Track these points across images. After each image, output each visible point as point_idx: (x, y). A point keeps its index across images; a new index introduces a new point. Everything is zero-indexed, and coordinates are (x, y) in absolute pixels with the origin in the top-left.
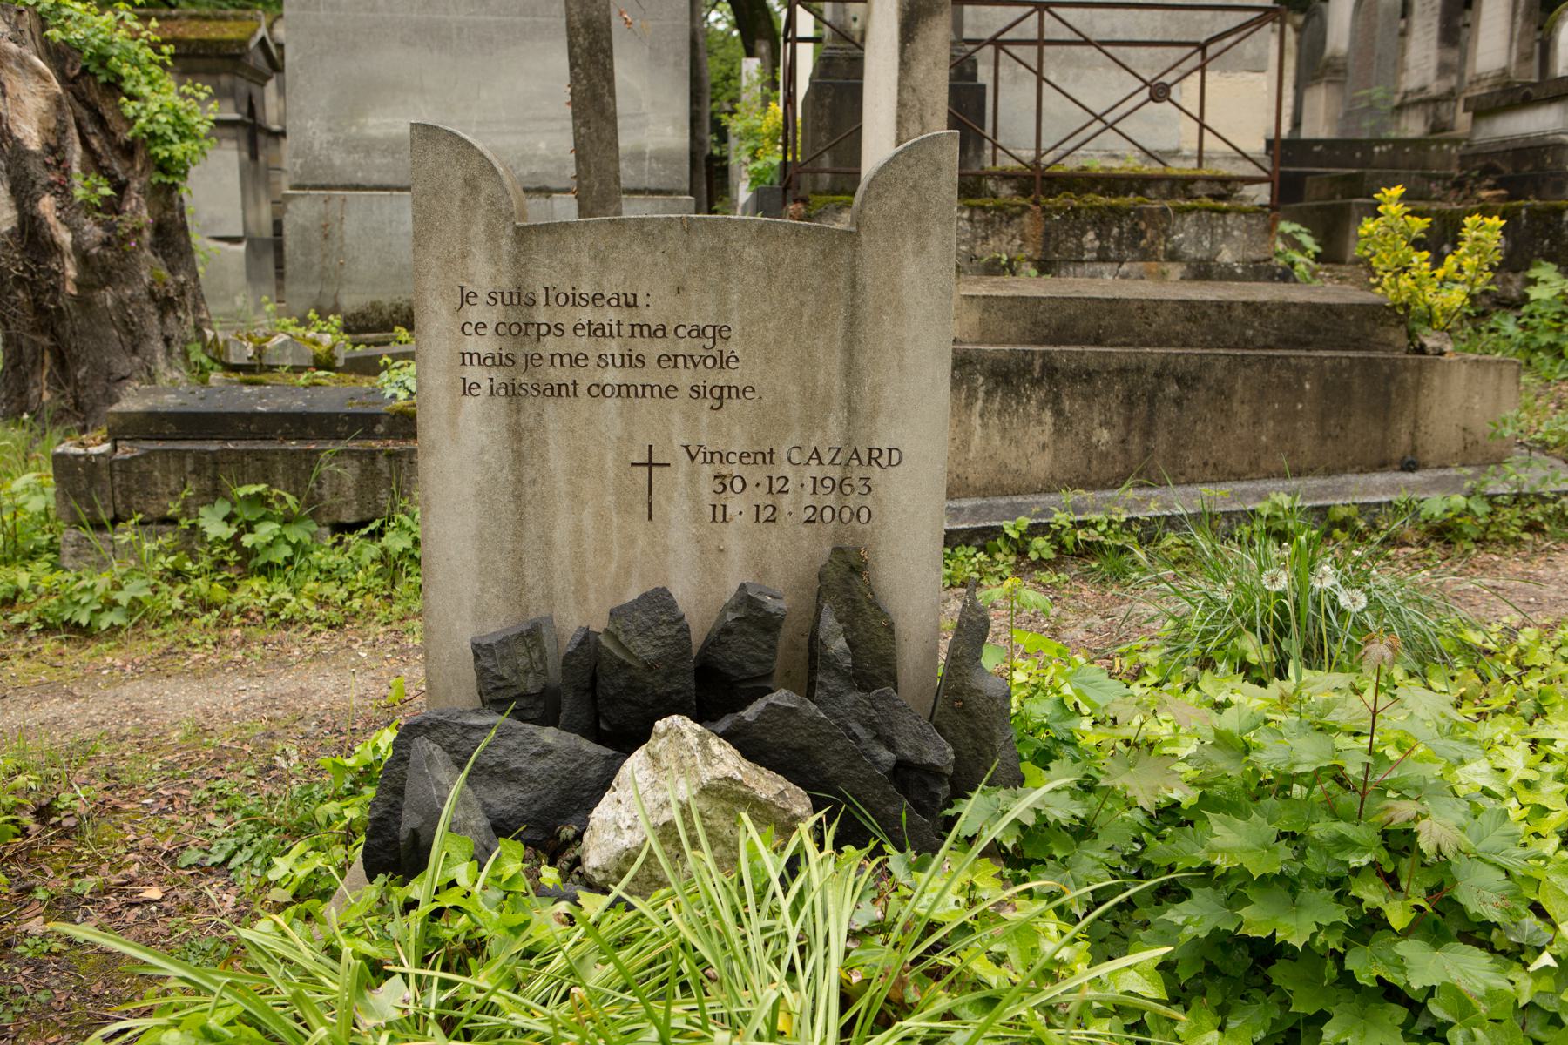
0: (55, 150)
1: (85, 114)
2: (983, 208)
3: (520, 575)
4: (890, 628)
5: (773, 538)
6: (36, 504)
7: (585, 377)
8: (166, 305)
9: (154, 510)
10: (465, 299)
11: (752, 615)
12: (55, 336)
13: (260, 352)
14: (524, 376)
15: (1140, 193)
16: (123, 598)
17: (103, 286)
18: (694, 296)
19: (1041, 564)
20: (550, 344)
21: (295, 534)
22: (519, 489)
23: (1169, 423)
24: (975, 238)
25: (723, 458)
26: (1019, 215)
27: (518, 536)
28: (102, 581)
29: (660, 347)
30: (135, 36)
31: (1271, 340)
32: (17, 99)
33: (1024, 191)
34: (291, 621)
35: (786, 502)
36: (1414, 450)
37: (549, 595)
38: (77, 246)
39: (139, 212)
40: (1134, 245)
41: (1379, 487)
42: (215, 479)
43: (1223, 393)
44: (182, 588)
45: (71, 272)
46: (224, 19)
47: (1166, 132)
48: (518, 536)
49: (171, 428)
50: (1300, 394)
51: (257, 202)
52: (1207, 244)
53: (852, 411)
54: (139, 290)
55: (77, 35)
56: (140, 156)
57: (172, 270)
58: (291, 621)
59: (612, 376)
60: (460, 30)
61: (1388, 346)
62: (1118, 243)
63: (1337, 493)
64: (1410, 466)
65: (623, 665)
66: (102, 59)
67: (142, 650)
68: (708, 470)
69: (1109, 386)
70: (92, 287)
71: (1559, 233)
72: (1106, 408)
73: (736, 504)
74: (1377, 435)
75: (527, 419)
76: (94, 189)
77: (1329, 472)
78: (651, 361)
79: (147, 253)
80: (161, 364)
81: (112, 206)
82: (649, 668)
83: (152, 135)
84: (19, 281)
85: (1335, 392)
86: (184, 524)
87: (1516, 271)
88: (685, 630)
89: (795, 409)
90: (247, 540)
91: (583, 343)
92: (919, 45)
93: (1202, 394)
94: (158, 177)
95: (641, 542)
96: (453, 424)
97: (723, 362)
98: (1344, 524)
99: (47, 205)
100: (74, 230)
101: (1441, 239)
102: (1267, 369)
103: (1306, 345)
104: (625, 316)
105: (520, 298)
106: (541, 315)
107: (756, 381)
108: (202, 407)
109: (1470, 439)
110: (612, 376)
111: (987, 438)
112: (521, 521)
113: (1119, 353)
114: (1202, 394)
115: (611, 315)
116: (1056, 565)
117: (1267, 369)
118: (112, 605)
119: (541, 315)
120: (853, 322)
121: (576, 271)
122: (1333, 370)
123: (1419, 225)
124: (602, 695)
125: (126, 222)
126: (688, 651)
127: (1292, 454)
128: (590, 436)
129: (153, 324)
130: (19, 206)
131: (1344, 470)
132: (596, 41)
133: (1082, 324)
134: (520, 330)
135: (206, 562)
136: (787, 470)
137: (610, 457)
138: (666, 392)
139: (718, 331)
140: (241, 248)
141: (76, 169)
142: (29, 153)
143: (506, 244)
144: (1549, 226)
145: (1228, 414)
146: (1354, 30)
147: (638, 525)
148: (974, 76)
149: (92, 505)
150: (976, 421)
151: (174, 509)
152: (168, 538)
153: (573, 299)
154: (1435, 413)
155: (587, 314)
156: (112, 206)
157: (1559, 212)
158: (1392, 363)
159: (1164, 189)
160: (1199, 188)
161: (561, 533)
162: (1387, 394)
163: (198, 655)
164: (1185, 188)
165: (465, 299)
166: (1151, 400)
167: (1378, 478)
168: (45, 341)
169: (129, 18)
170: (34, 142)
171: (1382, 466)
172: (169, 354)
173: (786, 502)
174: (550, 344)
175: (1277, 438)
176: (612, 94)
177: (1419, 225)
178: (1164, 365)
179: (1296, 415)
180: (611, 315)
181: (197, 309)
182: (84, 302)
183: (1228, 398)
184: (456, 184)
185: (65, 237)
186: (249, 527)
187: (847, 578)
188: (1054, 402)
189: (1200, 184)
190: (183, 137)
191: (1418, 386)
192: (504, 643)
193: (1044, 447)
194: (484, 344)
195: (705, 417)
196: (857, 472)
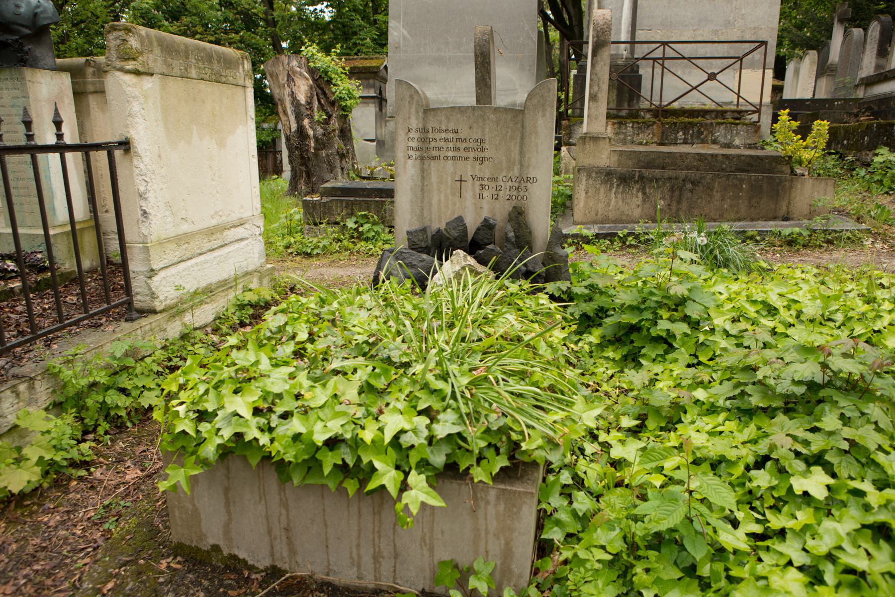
0: (309, 103)
1: (320, 91)
2: (638, 123)
3: (422, 213)
4: (530, 233)
5: (497, 205)
6: (297, 217)
7: (443, 154)
8: (342, 156)
9: (332, 219)
10: (409, 131)
11: (487, 226)
12: (307, 167)
13: (372, 172)
14: (425, 154)
15: (703, 117)
16: (321, 245)
17: (322, 149)
18: (475, 130)
19: (630, 246)
20: (433, 144)
21: (376, 228)
22: (423, 188)
23: (687, 199)
24: (634, 134)
25: (483, 179)
26: (652, 125)
27: (422, 202)
28: (315, 240)
29: (464, 145)
30: (337, 65)
31: (733, 169)
32: (299, 87)
33: (656, 116)
34: (372, 255)
35: (501, 193)
36: (788, 213)
37: (430, 220)
38: (314, 136)
39: (335, 124)
40: (698, 137)
41: (771, 226)
42: (352, 209)
43: (709, 188)
44: (339, 244)
45: (313, 145)
46: (372, 59)
47: (718, 95)
48: (422, 202)
49: (339, 193)
50: (741, 189)
51: (381, 126)
52: (729, 137)
53: (522, 165)
54: (334, 151)
55: (318, 65)
56: (337, 105)
57: (345, 145)
58: (372, 255)
59: (450, 154)
60: (450, 59)
61: (782, 172)
62: (692, 136)
63: (751, 227)
64: (786, 219)
65: (448, 239)
66: (326, 72)
67: (325, 261)
68: (478, 183)
69: (664, 184)
70: (319, 150)
71: (891, 134)
72: (663, 192)
73: (486, 194)
74: (773, 206)
75: (426, 167)
76: (321, 116)
77: (752, 220)
78: (462, 149)
79: (337, 138)
80: (340, 177)
81: (327, 122)
82: (455, 239)
83: (341, 98)
84: (297, 148)
85: (756, 190)
86: (342, 224)
87: (870, 151)
88: (466, 228)
89: (504, 164)
90: (361, 229)
91: (442, 144)
92: (599, 58)
93: (701, 188)
94: (342, 112)
95: (458, 204)
96: (405, 168)
97: (483, 150)
98: (751, 238)
99: (306, 122)
100: (314, 130)
101: (804, 131)
102: (728, 179)
103: (748, 171)
104: (454, 135)
105: (424, 130)
106: (430, 135)
107: (493, 156)
108: (349, 186)
109: (812, 209)
110: (450, 154)
111: (617, 202)
112: (423, 197)
113: (669, 173)
114: (701, 188)
115: (451, 135)
116: (636, 247)
117: (728, 179)
118: (317, 247)
119: (430, 135)
120: (522, 138)
121: (441, 122)
122: (755, 180)
123: (795, 124)
124: (440, 245)
125: (330, 128)
126: (466, 235)
127: (737, 212)
128: (444, 172)
129: (338, 163)
130: (298, 123)
131: (758, 219)
132: (484, 59)
133: (657, 161)
134: (424, 140)
135: (347, 236)
136: (502, 183)
137: (449, 178)
138: (466, 159)
139: (482, 141)
140: (375, 144)
141: (316, 110)
142: (301, 105)
143: (421, 114)
144: (887, 131)
145: (711, 196)
146: (841, 52)
147: (457, 199)
148: (638, 72)
149: (313, 217)
150: (613, 196)
151: (339, 219)
152: (337, 229)
153: (440, 131)
154: (797, 199)
155: (443, 135)
156: (327, 122)
157: (892, 125)
158: (780, 179)
159: (713, 115)
160: (728, 115)
161: (435, 201)
162: (778, 191)
163: (342, 262)
164: (722, 115)
165: (409, 131)
166: (681, 190)
167: (771, 223)
168: (304, 168)
169: (335, 58)
170: (303, 102)
171: (774, 218)
172: (343, 174)
173: (501, 193)
174: (433, 144)
175: (731, 206)
176: (490, 78)
177: (795, 124)
178: (686, 177)
179: (739, 197)
180: (451, 135)
181: (353, 159)
182: (316, 155)
183: (712, 190)
184: (407, 97)
185: (311, 133)
186: (362, 225)
187: (518, 216)
188: (643, 190)
189: (729, 113)
190: (350, 98)
191: (791, 187)
192: (416, 232)
193: (638, 206)
194: (414, 144)
195: (478, 167)
196: (523, 185)
